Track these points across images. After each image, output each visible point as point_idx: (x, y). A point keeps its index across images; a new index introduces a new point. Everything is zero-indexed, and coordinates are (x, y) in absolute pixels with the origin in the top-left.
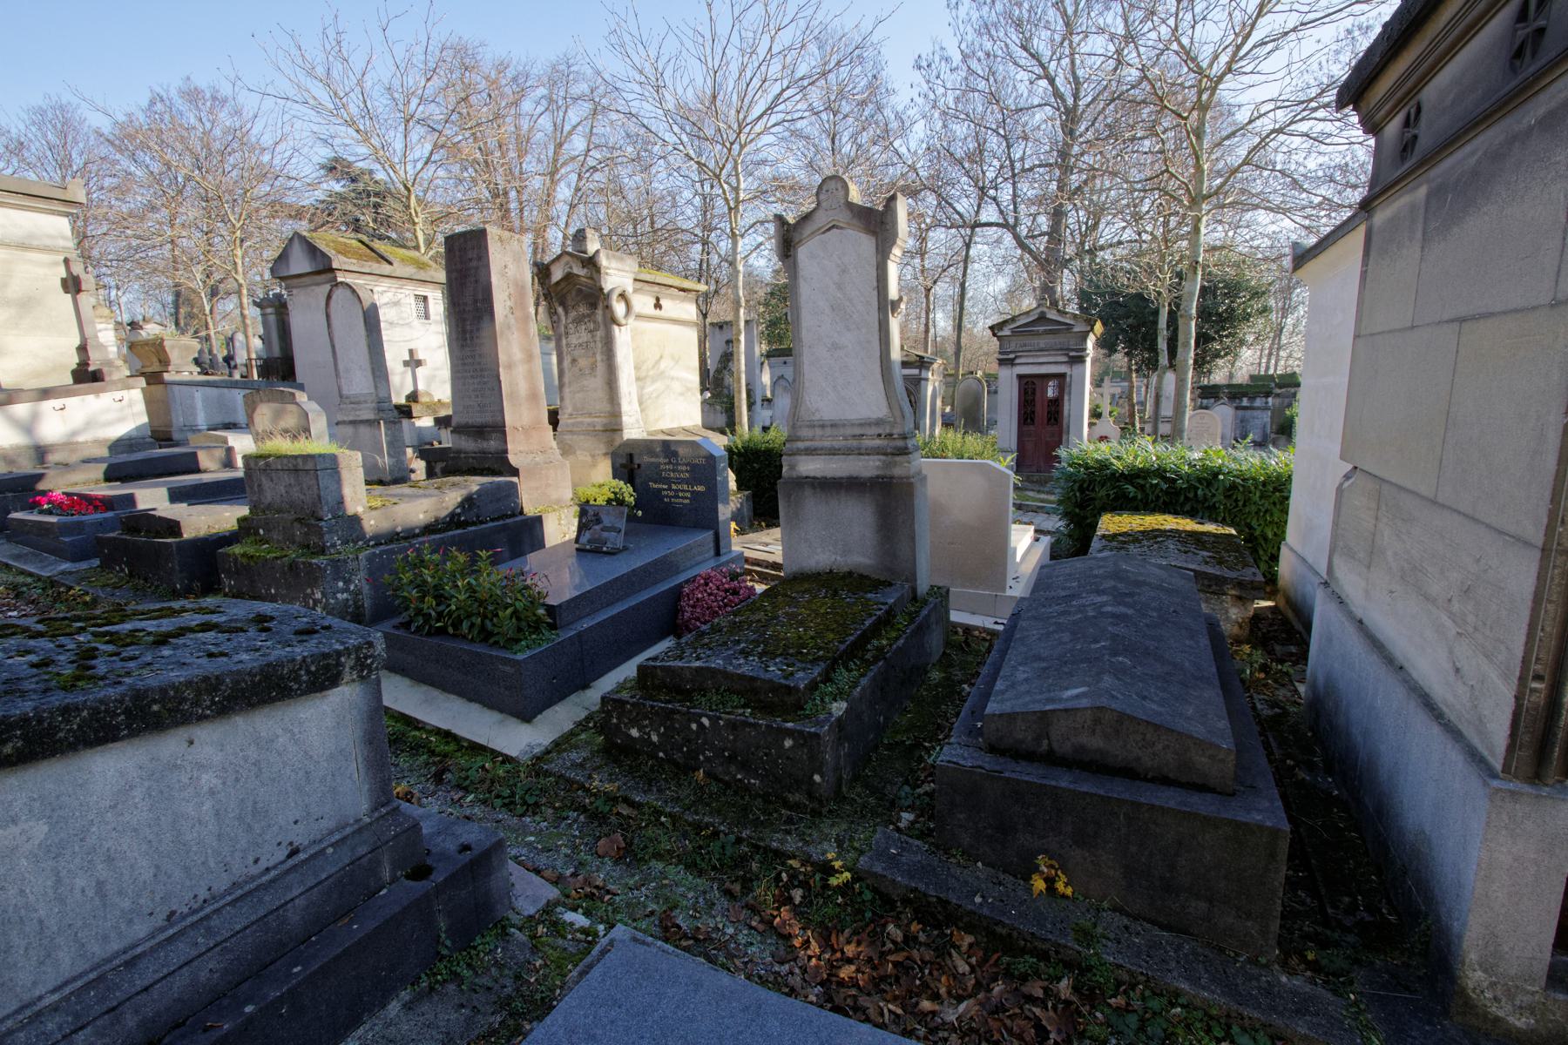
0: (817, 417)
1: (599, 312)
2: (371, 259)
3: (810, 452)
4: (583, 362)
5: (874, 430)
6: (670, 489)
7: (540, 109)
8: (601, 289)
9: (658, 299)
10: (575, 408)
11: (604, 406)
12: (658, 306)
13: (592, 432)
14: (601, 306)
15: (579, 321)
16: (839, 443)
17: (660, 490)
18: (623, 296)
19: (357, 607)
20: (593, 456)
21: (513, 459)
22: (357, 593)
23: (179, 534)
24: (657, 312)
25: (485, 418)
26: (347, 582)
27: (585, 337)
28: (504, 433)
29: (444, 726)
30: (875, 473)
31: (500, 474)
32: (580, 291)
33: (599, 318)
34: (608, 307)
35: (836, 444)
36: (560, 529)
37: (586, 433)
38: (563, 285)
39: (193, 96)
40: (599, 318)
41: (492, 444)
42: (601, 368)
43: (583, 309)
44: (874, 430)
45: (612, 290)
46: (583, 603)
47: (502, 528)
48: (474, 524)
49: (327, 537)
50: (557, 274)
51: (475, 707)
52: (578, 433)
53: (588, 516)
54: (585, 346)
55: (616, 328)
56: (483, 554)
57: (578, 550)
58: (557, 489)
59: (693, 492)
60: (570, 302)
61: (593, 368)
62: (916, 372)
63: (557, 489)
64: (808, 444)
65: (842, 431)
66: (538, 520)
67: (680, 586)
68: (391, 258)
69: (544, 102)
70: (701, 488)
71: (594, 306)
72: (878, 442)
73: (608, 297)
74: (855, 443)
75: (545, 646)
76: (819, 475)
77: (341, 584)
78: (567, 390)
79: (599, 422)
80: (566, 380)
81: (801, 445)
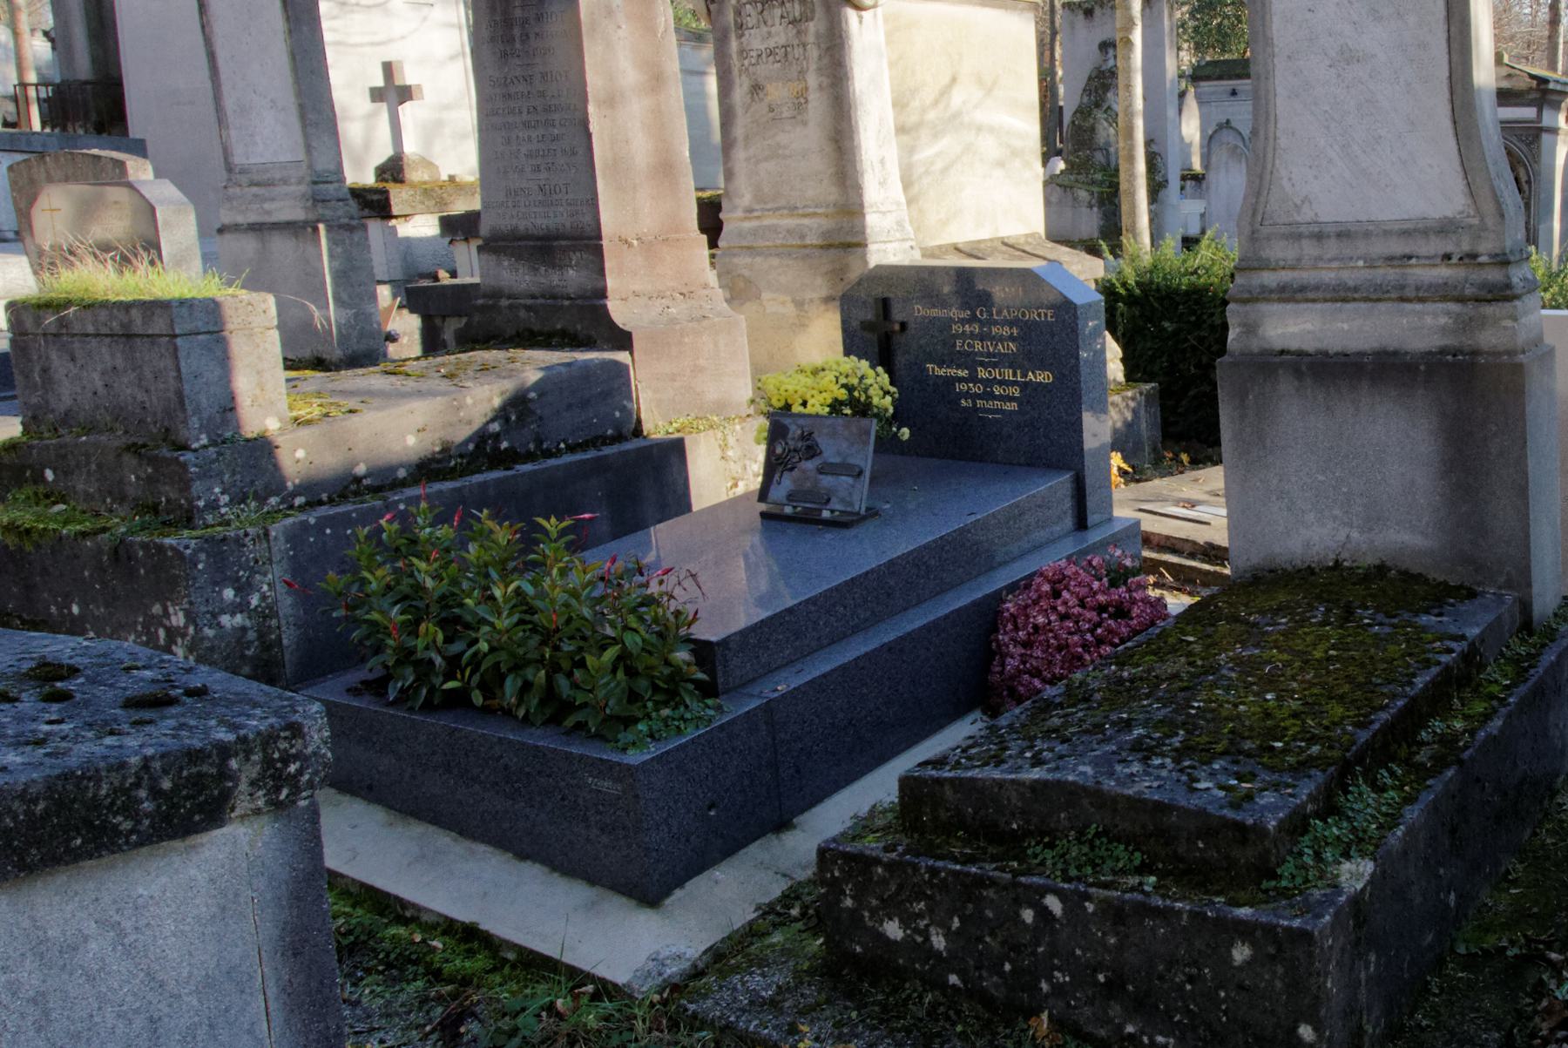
0: (1307, 214)
3: (1290, 294)
4: (778, 92)
5: (1436, 246)
6: (973, 378)
10: (759, 197)
11: (821, 190)
13: (798, 250)
19: (266, 646)
20: (799, 304)
21: (619, 311)
22: (266, 613)
26: (243, 589)
27: (781, 34)
28: (598, 252)
35: (1349, 277)
36: (726, 470)
37: (783, 252)
41: (572, 278)
42: (817, 103)
49: (197, 487)
51: (532, 872)
53: (788, 438)
54: (782, 55)
55: (851, 13)
56: (552, 525)
58: (719, 379)
59: (1024, 386)
62: (1529, 113)
63: (719, 379)
64: (1285, 276)
65: (1362, 247)
70: (1043, 377)
72: (1443, 273)
75: (691, 733)
76: (1310, 346)
77: (229, 593)
78: (740, 154)
79: (814, 227)
80: (739, 131)
81: (1269, 279)
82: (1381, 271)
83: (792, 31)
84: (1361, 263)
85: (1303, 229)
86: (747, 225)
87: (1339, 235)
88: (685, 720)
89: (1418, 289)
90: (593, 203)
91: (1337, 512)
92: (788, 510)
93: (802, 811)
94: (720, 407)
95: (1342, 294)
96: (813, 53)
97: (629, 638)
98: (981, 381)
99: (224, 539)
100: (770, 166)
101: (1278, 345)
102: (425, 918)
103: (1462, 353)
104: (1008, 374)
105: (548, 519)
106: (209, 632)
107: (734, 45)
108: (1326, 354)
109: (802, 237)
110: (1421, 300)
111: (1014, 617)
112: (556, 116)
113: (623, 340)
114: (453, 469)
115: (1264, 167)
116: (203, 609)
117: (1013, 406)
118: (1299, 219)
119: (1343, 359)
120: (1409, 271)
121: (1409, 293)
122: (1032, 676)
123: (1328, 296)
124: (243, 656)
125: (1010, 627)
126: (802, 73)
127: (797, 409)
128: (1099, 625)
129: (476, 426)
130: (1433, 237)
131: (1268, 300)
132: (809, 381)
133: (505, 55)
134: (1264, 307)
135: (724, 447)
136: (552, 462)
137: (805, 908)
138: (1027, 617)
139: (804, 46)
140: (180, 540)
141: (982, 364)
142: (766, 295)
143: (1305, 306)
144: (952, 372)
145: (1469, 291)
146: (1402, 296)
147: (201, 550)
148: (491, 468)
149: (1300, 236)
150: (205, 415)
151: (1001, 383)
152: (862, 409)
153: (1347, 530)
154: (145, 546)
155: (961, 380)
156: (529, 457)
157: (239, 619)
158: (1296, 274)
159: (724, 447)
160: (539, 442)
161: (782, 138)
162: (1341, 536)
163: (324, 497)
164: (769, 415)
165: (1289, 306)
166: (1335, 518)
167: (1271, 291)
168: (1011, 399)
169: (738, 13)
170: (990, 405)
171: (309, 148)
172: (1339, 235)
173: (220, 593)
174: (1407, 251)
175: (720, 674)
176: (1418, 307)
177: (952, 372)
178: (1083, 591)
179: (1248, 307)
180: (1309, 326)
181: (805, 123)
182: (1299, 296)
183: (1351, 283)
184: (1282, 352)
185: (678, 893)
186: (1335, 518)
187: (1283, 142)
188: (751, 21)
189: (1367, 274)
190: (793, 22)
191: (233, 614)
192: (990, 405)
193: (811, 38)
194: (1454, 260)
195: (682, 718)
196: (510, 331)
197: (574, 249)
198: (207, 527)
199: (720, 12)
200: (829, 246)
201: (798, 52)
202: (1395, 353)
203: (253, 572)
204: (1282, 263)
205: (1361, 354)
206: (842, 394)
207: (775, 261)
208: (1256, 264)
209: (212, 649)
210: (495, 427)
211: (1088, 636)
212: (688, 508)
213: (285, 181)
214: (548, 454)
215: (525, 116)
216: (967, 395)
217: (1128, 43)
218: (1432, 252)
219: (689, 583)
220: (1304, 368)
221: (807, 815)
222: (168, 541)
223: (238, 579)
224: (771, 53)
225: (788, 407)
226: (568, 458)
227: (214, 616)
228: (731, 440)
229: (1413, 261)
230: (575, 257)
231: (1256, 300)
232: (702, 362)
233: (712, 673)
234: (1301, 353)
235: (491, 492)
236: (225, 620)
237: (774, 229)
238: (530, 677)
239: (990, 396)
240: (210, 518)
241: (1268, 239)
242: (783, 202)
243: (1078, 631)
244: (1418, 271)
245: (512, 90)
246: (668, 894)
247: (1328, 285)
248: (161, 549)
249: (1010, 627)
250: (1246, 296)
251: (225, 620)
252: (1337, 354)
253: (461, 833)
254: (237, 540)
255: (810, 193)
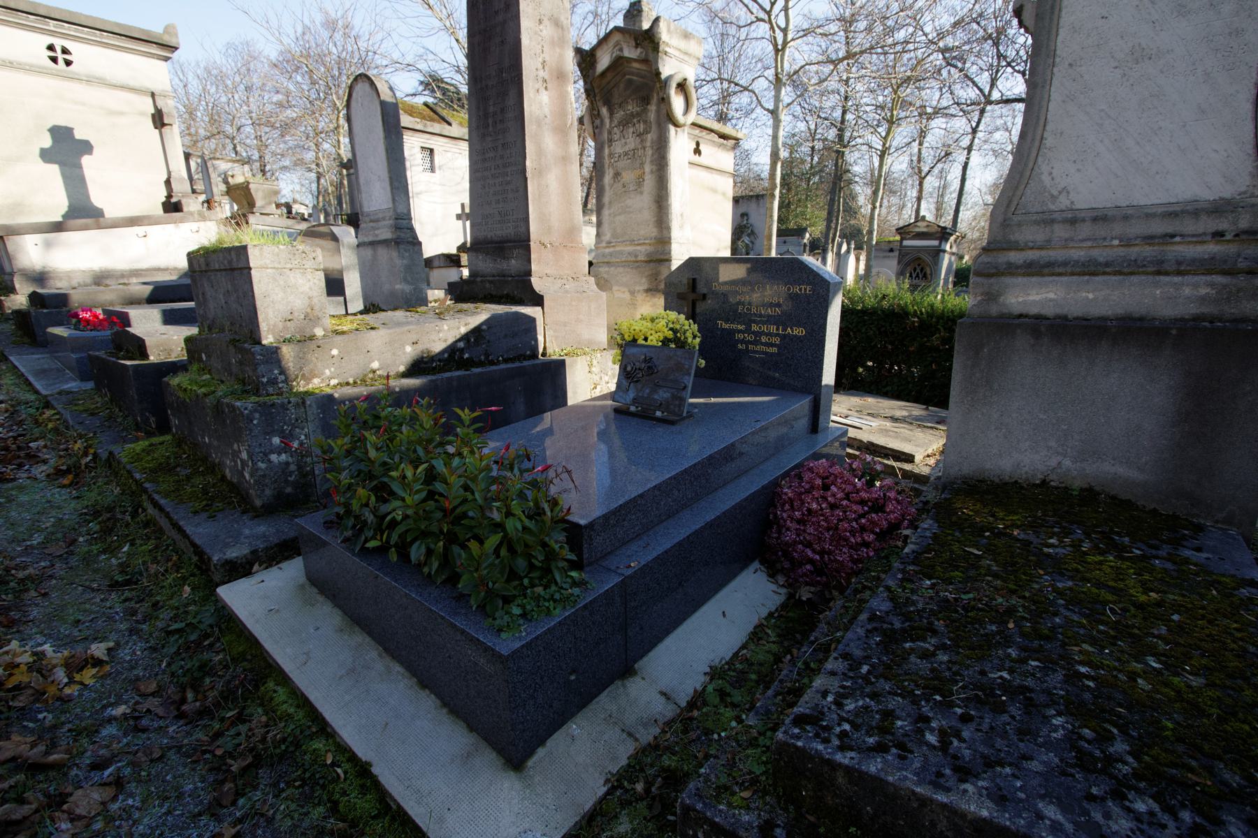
0: (1064, 202)
1: (653, 108)
2: (432, 120)
3: (1034, 270)
4: (628, 176)
5: (1209, 224)
6: (748, 330)
7: (587, 23)
8: (658, 74)
9: (698, 144)
10: (614, 235)
11: (651, 231)
12: (697, 151)
13: (635, 264)
14: (655, 100)
15: (625, 123)
16: (1114, 251)
17: (732, 332)
18: (682, 86)
19: (303, 475)
20: (632, 293)
21: (537, 284)
22: (302, 453)
23: (144, 355)
24: (696, 158)
25: (507, 231)
26: (287, 438)
27: (632, 142)
28: (528, 249)
29: (362, 753)
30: (1193, 309)
31: (520, 302)
32: (630, 82)
33: (652, 116)
34: (665, 101)
35: (1100, 254)
36: (592, 379)
37: (625, 264)
38: (609, 76)
39: (331, 25)
40: (652, 116)
41: (514, 264)
42: (649, 182)
43: (632, 107)
44: (1190, 226)
45: (670, 78)
46: (630, 517)
47: (501, 376)
48: (481, 364)
49: (262, 369)
50: (604, 62)
51: (428, 701)
52: (616, 265)
53: (638, 362)
54: (631, 155)
55: (672, 129)
56: (466, 415)
57: (617, 411)
58: (586, 338)
59: (783, 337)
60: (616, 100)
61: (640, 182)
62: (936, 243)
63: (586, 338)
64: (1032, 255)
65: (1118, 228)
66: (562, 364)
67: (775, 483)
68: (450, 120)
69: (590, 18)
70: (799, 331)
71: (646, 101)
72: (1212, 248)
73: (665, 84)
74: (1148, 251)
75: (559, 614)
76: (1049, 311)
77: (276, 440)
78: (606, 212)
79: (642, 251)
80: (606, 200)
81: (1015, 257)
82: (1136, 249)
83: (638, 140)
84: (1116, 242)
85: (1056, 216)
86: (607, 250)
87: (1095, 220)
88: (555, 601)
89: (1179, 263)
90: (526, 220)
91: (1053, 444)
92: (633, 409)
93: (642, 657)
94: (590, 343)
95: (1092, 269)
96: (649, 152)
97: (511, 524)
98: (753, 333)
99: (273, 405)
100: (622, 218)
101: (1017, 310)
102: (665, 232)
103: (1220, 321)
104: (773, 329)
105: (463, 410)
106: (262, 465)
107: (606, 151)
108: (1065, 318)
109: (636, 256)
110: (1179, 273)
111: (791, 501)
112: (509, 170)
113: (538, 300)
114: (434, 368)
115: (1026, 165)
116: (257, 450)
117: (775, 350)
118: (1053, 207)
119: (1085, 323)
120: (1169, 248)
121: (1166, 267)
122: (806, 546)
123: (1078, 270)
124: (286, 481)
125: (787, 507)
126: (642, 164)
127: (641, 342)
128: (863, 516)
129: (450, 341)
130: (1204, 217)
131: (1012, 275)
132: (649, 324)
133: (484, 136)
134: (1008, 280)
135: (591, 366)
136: (494, 368)
137: (649, 785)
138: (803, 502)
139: (644, 148)
140: (246, 404)
141: (754, 322)
142: (615, 288)
143: (1051, 278)
144: (734, 326)
145: (1242, 264)
146: (1159, 269)
147: (256, 411)
148: (458, 369)
149: (1053, 221)
150: (272, 323)
151: (767, 335)
152: (681, 344)
153: (1060, 458)
154: (228, 405)
155: (740, 331)
156: (481, 364)
157: (283, 457)
158: (1043, 253)
159: (591, 366)
160: (487, 355)
161: (629, 202)
162: (1053, 462)
163: (351, 381)
164: (620, 346)
165: (1034, 279)
166: (1049, 448)
167: (1018, 267)
168: (772, 345)
169: (610, 133)
170: (758, 348)
171: (394, 200)
172: (1095, 220)
173: (270, 440)
174: (1170, 230)
175: (585, 551)
176: (1177, 279)
177: (734, 326)
178: (849, 488)
179: (992, 280)
180: (1052, 295)
181: (641, 193)
182: (1046, 271)
183: (1101, 260)
184: (1021, 316)
185: (541, 752)
186: (1049, 448)
187: (1050, 141)
188: (616, 137)
189: (1122, 252)
190: (639, 135)
191: (279, 454)
192: (758, 348)
193: (648, 144)
194: (1228, 237)
195: (552, 598)
196: (481, 296)
197: (515, 247)
198: (268, 395)
199: (601, 133)
200: (650, 261)
201: (640, 152)
202: (1141, 319)
203: (294, 427)
204: (1031, 244)
205: (1104, 319)
206: (670, 334)
207: (621, 270)
208: (1005, 246)
209: (264, 476)
210: (461, 345)
211: (854, 524)
212: (566, 404)
213: (384, 219)
214: (492, 363)
215: (493, 171)
216: (742, 342)
217: (773, 196)
218: (1201, 231)
219: (565, 476)
220: (1043, 329)
221: (645, 659)
222: (238, 404)
223: (283, 431)
224: (626, 154)
225: (635, 340)
226: (503, 366)
227: (266, 455)
228: (595, 362)
229: (1178, 239)
230: (515, 252)
231: (1003, 274)
232: (581, 317)
233: (580, 555)
234: (1038, 317)
235: (455, 383)
236: (274, 457)
237: (621, 253)
238: (432, 546)
239: (756, 343)
240: (271, 390)
241: (1019, 225)
242: (627, 237)
243: (846, 518)
244: (1180, 248)
245: (487, 156)
246: (531, 753)
247: (1077, 262)
248: (233, 406)
249: (787, 507)
250: (994, 271)
251: (274, 457)
252: (1077, 318)
253: (386, 650)
254: (282, 405)
255: (642, 232)
